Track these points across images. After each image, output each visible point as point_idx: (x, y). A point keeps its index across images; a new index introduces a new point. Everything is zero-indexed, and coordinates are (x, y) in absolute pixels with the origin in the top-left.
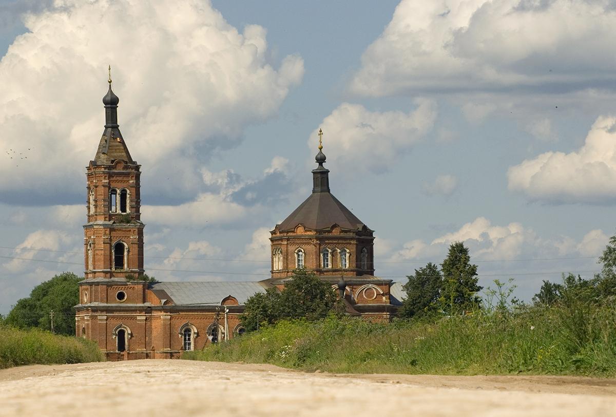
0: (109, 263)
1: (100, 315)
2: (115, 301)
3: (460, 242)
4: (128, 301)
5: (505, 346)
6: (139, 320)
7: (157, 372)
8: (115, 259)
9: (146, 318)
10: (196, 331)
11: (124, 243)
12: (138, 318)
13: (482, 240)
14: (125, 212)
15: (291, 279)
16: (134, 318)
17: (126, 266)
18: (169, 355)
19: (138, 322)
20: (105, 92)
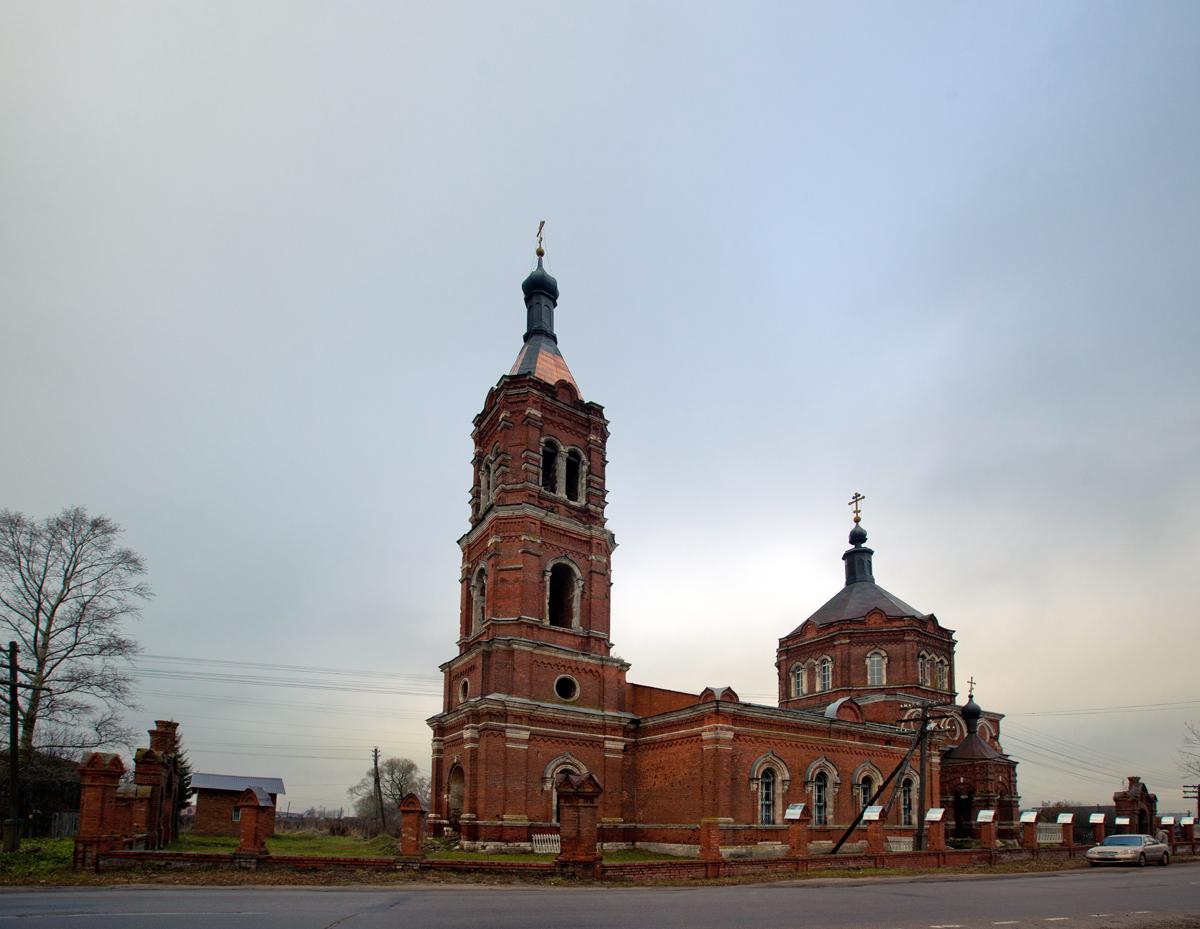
0: (565, 636)
1: (510, 728)
2: (549, 698)
3: (309, 809)
4: (584, 701)
5: (18, 868)
6: (611, 751)
7: (895, 894)
8: (550, 610)
9: (625, 747)
10: (787, 776)
11: (573, 566)
12: (609, 745)
13: (415, 780)
14: (575, 500)
15: (183, 830)
16: (600, 744)
17: (576, 621)
18: (730, 834)
19: (510, 746)
20: (504, 356)
